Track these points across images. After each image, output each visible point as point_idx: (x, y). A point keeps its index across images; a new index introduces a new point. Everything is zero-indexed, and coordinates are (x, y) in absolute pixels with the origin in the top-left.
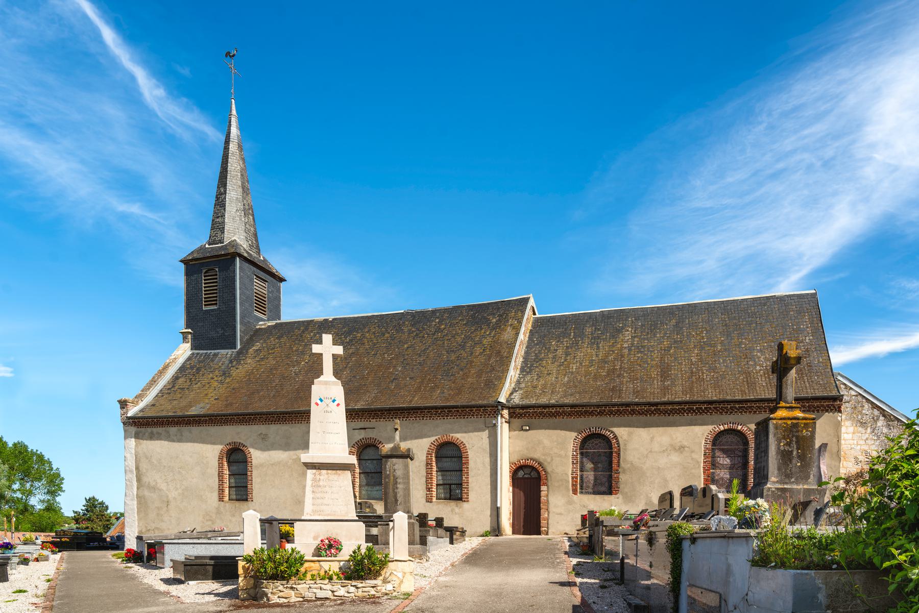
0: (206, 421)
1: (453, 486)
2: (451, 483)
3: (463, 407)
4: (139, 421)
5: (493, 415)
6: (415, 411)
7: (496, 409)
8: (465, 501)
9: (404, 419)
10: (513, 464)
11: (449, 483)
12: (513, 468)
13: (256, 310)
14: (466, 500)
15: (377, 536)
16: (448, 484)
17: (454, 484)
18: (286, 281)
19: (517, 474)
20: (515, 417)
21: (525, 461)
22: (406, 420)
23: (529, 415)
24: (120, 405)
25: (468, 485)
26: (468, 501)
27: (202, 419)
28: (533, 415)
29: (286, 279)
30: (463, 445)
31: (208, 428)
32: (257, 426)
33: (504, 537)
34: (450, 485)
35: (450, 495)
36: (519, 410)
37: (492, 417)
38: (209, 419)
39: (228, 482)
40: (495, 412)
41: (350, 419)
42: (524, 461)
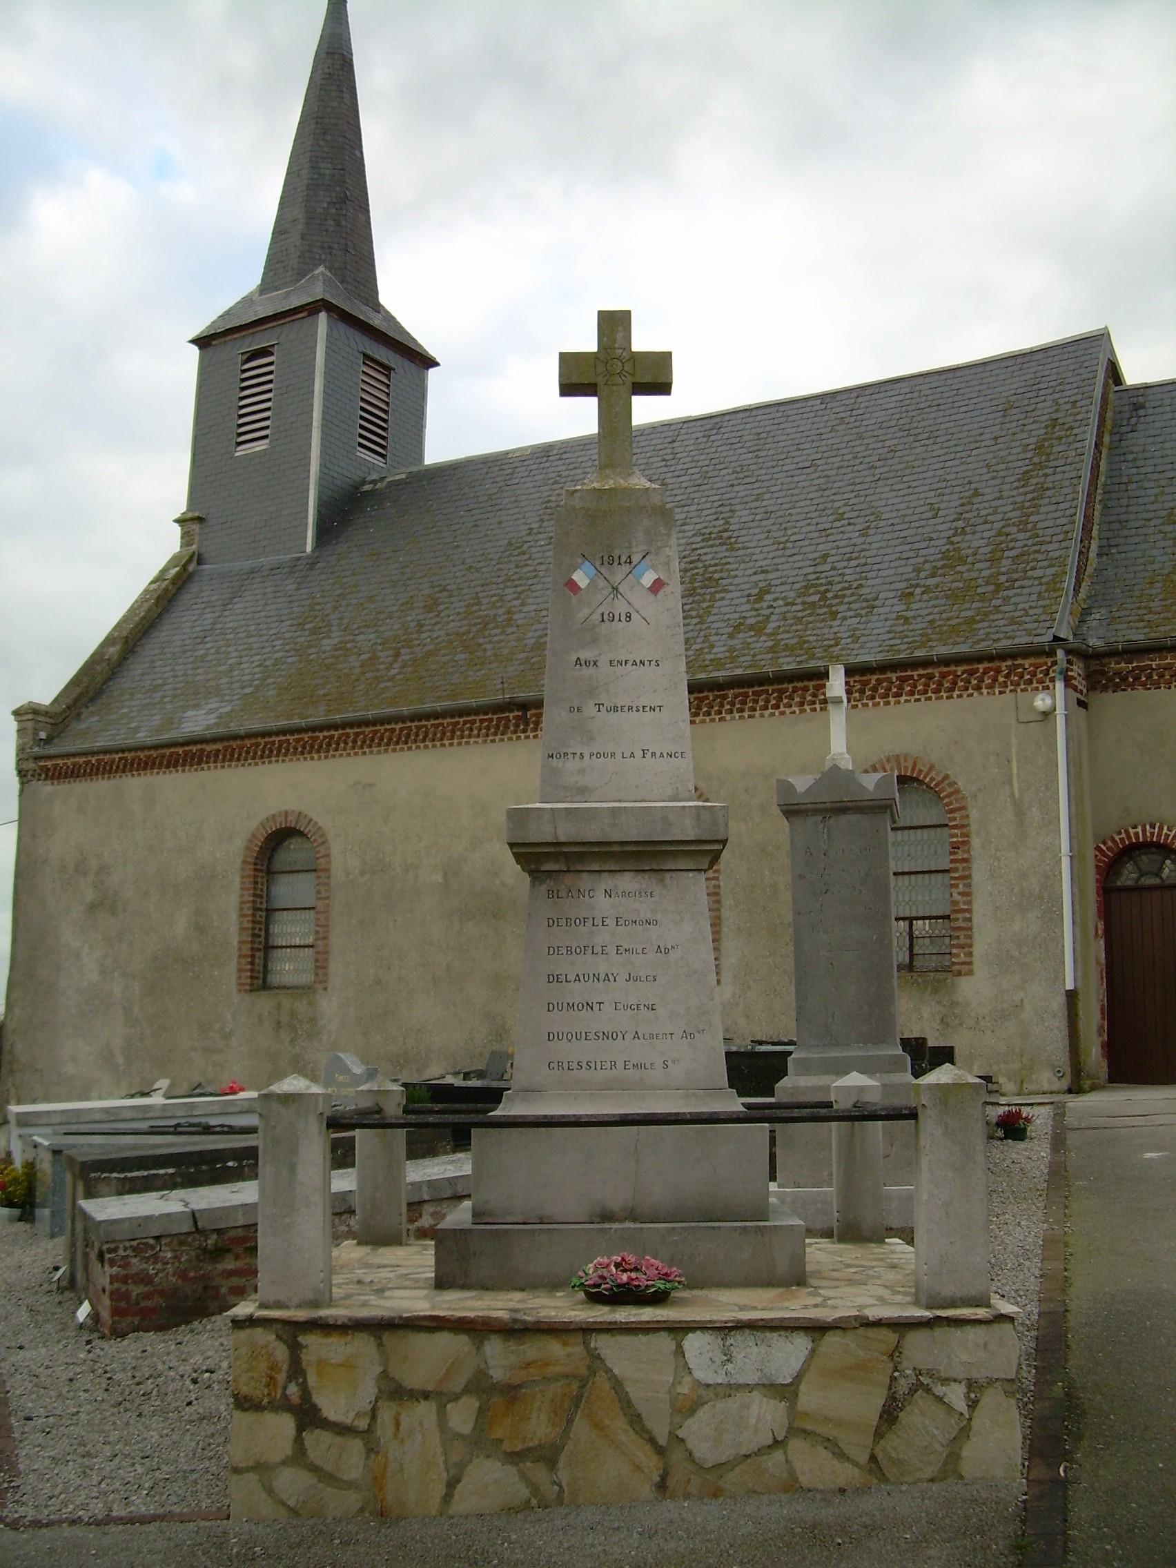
0: (217, 756)
1: (920, 922)
2: (914, 914)
3: (883, 668)
4: (55, 766)
5: (1041, 681)
6: (800, 684)
7: (1049, 661)
8: (959, 974)
9: (767, 713)
10: (1104, 843)
11: (907, 915)
12: (1105, 855)
13: (361, 445)
14: (964, 968)
15: (409, 1158)
16: (904, 919)
17: (923, 918)
18: (437, 364)
19: (1118, 874)
20: (1105, 688)
21: (1144, 831)
22: (906, 701)
23: (1149, 677)
24: (19, 721)
25: (970, 920)
26: (970, 973)
27: (321, 735)
28: (1161, 676)
29: (438, 360)
30: (950, 785)
31: (345, 762)
32: (410, 752)
33: (980, 1147)
34: (911, 920)
35: (912, 955)
36: (1118, 663)
37: (1037, 689)
38: (226, 748)
39: (263, 933)
40: (1047, 673)
41: (766, 708)
42: (1139, 829)
